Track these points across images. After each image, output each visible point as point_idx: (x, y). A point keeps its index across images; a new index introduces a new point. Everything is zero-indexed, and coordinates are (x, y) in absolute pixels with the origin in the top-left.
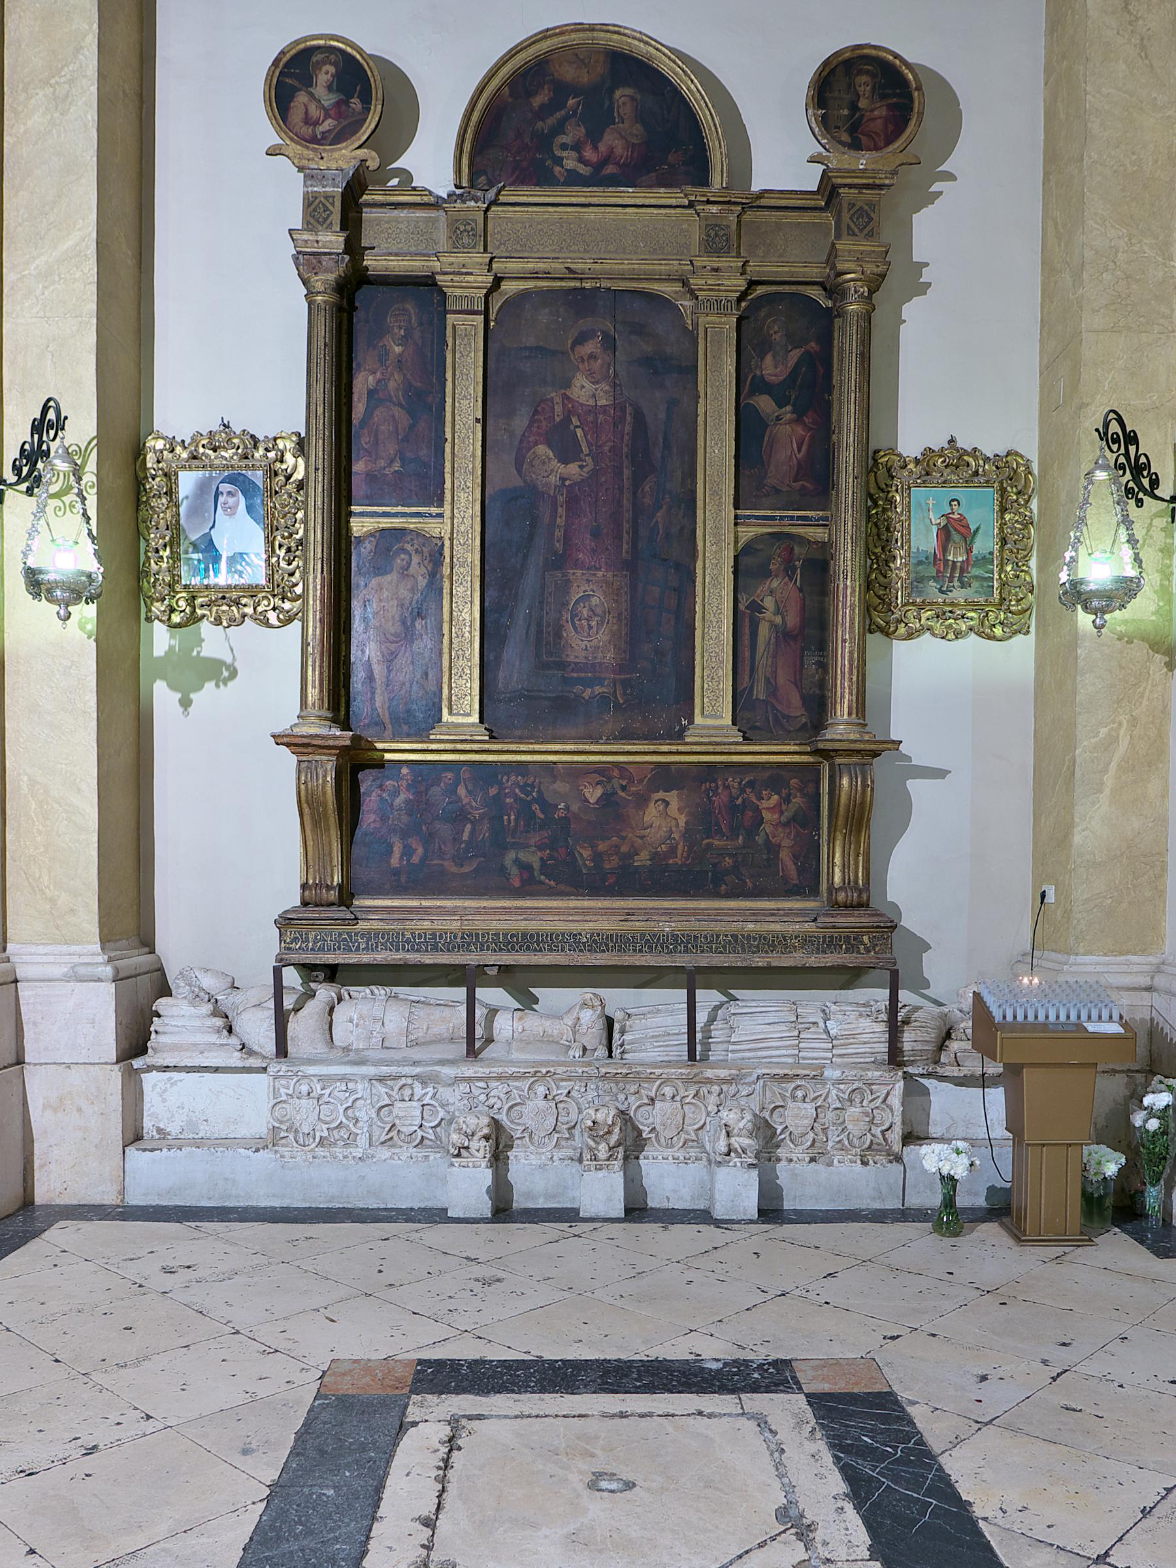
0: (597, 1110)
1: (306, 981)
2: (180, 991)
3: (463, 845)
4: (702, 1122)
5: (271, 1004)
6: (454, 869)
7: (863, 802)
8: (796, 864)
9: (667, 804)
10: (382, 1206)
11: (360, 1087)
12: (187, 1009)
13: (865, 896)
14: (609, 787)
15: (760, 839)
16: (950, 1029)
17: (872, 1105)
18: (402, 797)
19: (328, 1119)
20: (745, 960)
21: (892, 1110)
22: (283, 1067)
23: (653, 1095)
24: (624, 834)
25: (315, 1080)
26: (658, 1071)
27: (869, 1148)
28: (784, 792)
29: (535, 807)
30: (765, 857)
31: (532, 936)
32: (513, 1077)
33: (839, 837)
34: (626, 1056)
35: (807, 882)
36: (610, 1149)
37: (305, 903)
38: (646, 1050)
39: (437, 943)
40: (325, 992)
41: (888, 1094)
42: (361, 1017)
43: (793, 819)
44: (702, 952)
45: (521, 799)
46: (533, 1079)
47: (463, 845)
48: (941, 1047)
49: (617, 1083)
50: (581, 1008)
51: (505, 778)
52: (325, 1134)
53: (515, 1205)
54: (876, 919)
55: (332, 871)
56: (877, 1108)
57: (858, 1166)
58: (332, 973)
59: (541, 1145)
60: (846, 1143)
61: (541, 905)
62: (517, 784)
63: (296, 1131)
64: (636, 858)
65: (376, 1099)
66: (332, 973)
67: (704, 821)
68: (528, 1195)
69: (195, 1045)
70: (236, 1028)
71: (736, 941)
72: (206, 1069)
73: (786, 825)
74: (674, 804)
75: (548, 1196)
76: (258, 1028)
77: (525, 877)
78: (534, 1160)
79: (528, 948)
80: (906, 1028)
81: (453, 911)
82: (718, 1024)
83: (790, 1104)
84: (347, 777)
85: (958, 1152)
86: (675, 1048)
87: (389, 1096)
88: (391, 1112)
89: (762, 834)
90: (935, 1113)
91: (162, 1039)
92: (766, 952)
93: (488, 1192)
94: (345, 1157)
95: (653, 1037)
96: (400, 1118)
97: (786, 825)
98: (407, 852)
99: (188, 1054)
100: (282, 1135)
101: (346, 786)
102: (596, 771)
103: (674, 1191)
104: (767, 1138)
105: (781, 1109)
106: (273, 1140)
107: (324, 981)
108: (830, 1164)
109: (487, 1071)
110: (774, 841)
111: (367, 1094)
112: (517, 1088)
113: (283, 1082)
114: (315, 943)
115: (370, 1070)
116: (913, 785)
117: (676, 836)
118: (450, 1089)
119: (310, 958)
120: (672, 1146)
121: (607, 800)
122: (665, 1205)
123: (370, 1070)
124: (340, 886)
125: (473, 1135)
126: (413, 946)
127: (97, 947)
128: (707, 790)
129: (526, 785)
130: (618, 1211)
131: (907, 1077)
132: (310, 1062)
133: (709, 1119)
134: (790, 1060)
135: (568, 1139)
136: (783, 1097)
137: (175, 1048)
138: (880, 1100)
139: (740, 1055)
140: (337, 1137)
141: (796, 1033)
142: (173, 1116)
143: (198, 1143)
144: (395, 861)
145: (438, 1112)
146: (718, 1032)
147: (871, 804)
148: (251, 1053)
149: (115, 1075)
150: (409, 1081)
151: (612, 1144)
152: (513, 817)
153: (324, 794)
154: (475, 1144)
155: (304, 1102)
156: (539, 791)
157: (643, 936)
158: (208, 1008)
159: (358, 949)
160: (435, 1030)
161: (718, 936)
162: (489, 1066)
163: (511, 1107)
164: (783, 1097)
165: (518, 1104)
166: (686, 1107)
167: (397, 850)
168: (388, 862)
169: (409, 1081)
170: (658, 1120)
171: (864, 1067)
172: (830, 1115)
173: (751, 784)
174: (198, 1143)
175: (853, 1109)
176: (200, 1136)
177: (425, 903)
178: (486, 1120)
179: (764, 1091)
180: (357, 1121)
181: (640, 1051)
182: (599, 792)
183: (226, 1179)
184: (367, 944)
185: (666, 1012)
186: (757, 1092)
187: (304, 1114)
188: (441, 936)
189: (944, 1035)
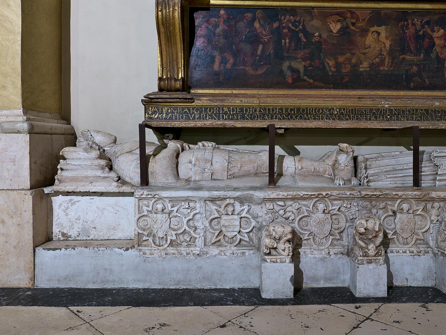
0: (367, 221)
1: (161, 139)
2: (81, 144)
3: (258, 58)
4: (427, 227)
5: (138, 151)
6: (252, 72)
9: (379, 34)
10: (213, 287)
11: (198, 205)
12: (83, 155)
14: (344, 23)
19: (176, 227)
20: (434, 124)
22: (145, 192)
23: (396, 209)
24: (354, 52)
25: (167, 201)
26: (400, 193)
29: (301, 35)
30: (436, 66)
31: (303, 110)
32: (303, 198)
34: (371, 184)
36: (376, 247)
37: (161, 89)
38: (381, 180)
39: (244, 115)
40: (173, 145)
42: (197, 159)
44: (407, 120)
45: (292, 30)
47: (258, 58)
49: (371, 202)
50: (338, 154)
51: (283, 17)
52: (174, 238)
53: (304, 286)
55: (178, 70)
58: (177, 133)
59: (321, 244)
61: (305, 93)
62: (290, 21)
63: (154, 236)
64: (361, 66)
65: (208, 213)
66: (177, 133)
67: (401, 45)
68: (314, 279)
69: (86, 177)
70: (115, 167)
71: (428, 113)
72: (95, 194)
75: (327, 279)
76: (129, 167)
77: (295, 77)
78: (318, 255)
79: (301, 118)
81: (253, 96)
84: (187, 14)
86: (400, 179)
87: (218, 211)
88: (219, 223)
89: (435, 52)
91: (65, 174)
93: (291, 280)
94: (188, 254)
95: (386, 171)
96: (225, 227)
98: (224, 61)
99: (82, 183)
100: (145, 238)
101: (187, 19)
102: (338, 14)
103: (411, 274)
106: (137, 242)
107: (173, 139)
109: (285, 194)
110: (441, 56)
111: (203, 211)
112: (305, 205)
113: (145, 202)
114: (167, 114)
115: (205, 194)
117: (384, 53)
118: (260, 207)
119: (164, 124)
120: (407, 244)
121: (344, 31)
122: (405, 284)
123: (205, 194)
124: (183, 79)
125: (280, 239)
127: (20, 111)
128: (402, 26)
129: (295, 21)
130: (382, 292)
132: (164, 188)
133: (432, 225)
135: (338, 239)
137: (74, 179)
140: (182, 240)
142: (73, 225)
143: (87, 244)
144: (216, 66)
145: (251, 222)
148: (124, 183)
149: (28, 200)
150: (232, 201)
152: (287, 41)
153: (174, 17)
154: (281, 246)
155: (159, 216)
156: (303, 26)
158: (95, 153)
159: (194, 118)
160: (246, 168)
161: (417, 110)
162: (286, 191)
163: (301, 219)
167: (217, 60)
169: (232, 201)
173: (428, 23)
174: (87, 244)
176: (90, 238)
177: (235, 92)
178: (289, 229)
180: (196, 229)
181: (378, 181)
182: (339, 26)
183: (106, 269)
184: (200, 115)
185: (389, 156)
187: (160, 224)
188: (246, 110)
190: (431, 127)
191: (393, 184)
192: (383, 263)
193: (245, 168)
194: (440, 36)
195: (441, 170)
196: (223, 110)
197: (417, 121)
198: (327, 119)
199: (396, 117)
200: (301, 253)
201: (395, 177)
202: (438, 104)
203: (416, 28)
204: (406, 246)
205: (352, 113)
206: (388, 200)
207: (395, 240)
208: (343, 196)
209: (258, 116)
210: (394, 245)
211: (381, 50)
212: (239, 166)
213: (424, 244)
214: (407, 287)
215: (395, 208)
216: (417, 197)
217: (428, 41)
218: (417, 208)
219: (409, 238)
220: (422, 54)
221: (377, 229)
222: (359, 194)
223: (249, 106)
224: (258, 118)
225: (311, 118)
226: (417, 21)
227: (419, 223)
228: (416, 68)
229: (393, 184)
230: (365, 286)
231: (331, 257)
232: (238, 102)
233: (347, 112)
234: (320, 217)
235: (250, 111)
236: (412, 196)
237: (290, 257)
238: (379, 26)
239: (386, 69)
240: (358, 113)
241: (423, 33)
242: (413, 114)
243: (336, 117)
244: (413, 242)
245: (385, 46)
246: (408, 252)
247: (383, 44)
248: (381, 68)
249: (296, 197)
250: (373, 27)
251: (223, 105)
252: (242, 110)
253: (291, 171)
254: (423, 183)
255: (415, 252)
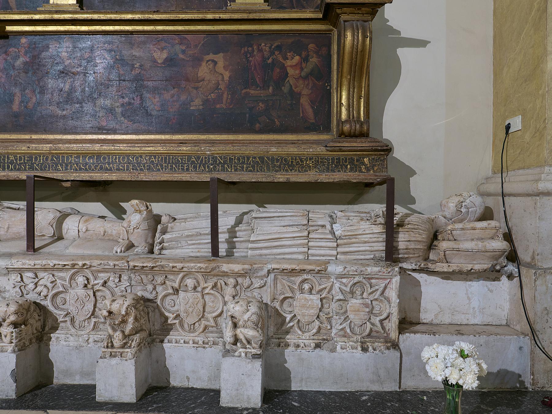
4: (219, 311)
7: (363, 50)
8: (313, 108)
9: (215, 63)
13: (365, 128)
15: (285, 89)
16: (436, 232)
17: (371, 297)
18: (22, 59)
20: (269, 176)
21: (389, 302)
26: (179, 265)
27: (369, 335)
28: (304, 54)
30: (289, 102)
33: (345, 82)
34: (164, 252)
35: (322, 121)
39: (33, 164)
41: (385, 288)
43: (311, 73)
46: (73, 271)
48: (431, 247)
53: (55, 381)
54: (374, 144)
56: (376, 300)
57: (358, 353)
60: (348, 331)
67: (243, 77)
68: (67, 373)
73: (305, 78)
74: (221, 64)
78: (72, 341)
79: (101, 168)
80: (400, 229)
82: (242, 227)
83: (298, 295)
85: (463, 355)
90: (425, 303)
92: (287, 171)
95: (188, 236)
97: (305, 78)
104: (274, 327)
105: (290, 300)
108: (333, 350)
109: (32, 263)
110: (296, 90)
116: (403, 53)
117: (222, 86)
118: (6, 278)
122: (185, 384)
126: (15, 167)
131: (403, 271)
134: (301, 257)
136: (292, 290)
138: (379, 293)
139: (258, 252)
141: (306, 234)
144: (15, 107)
146: (242, 233)
147: (370, 52)
151: (127, 332)
157: (189, 157)
161: (248, 158)
164: (292, 290)
165: (61, 292)
166: (207, 298)
168: (11, 108)
170: (182, 309)
171: (364, 263)
172: (334, 306)
173: (279, 48)
175: (354, 301)
179: (275, 284)
181: (177, 248)
182: (165, 55)
186: (268, 284)
189: (432, 236)
190: (264, 180)
191: (195, 252)
192: (131, 357)
193: (14, 229)
194: (294, 64)
195: (254, 236)
196: (8, 158)
197: (249, 171)
198: (133, 169)
199: (222, 167)
200: (53, 339)
201: (199, 244)
202: (275, 150)
203: (264, 54)
204: (192, 335)
205: (165, 162)
206: (171, 274)
207: (177, 325)
208: (106, 267)
209: (49, 166)
210: (176, 333)
211: (218, 84)
212: (6, 227)
213: (217, 332)
214: (188, 388)
215: (176, 285)
216: (203, 270)
217: (278, 70)
218: (206, 285)
219: (197, 324)
220: (271, 88)
221: (123, 313)
222: (126, 264)
223: (38, 153)
224: (49, 168)
225: (114, 168)
226: (265, 46)
227: (211, 304)
228: (263, 106)
229: (195, 252)
230: (105, 386)
231: (89, 345)
232: (23, 148)
233: (158, 160)
234: (78, 294)
235: (40, 160)
236: (195, 269)
237: (13, 344)
238: (215, 53)
239: (225, 107)
240: (172, 162)
241: (273, 62)
242: (243, 163)
243: (144, 166)
244: (201, 330)
245: (223, 78)
246: (191, 342)
247: (221, 76)
248: (218, 106)
249: (46, 267)
250: (209, 54)
251: (8, 153)
252: (31, 158)
253: (73, 233)
254: (236, 252)
255: (201, 342)
